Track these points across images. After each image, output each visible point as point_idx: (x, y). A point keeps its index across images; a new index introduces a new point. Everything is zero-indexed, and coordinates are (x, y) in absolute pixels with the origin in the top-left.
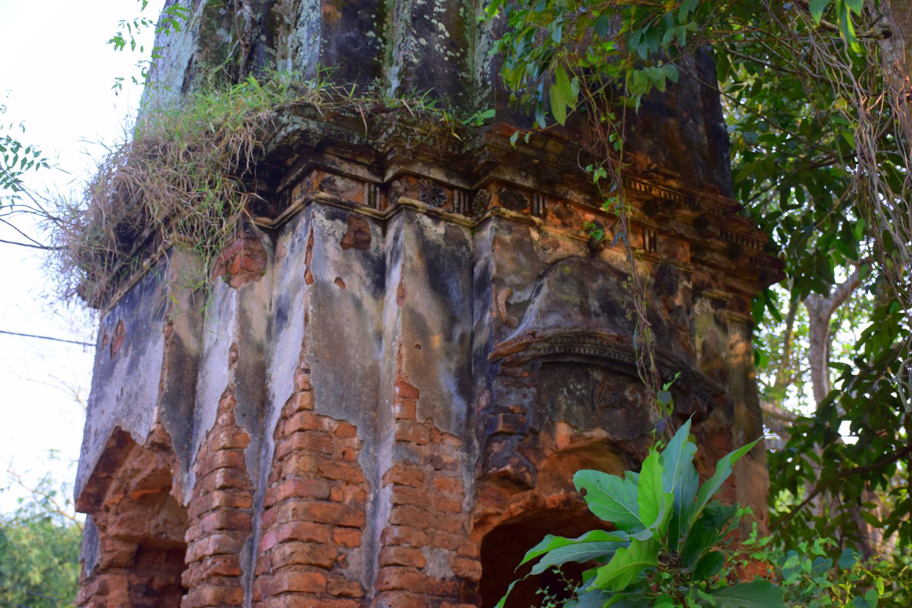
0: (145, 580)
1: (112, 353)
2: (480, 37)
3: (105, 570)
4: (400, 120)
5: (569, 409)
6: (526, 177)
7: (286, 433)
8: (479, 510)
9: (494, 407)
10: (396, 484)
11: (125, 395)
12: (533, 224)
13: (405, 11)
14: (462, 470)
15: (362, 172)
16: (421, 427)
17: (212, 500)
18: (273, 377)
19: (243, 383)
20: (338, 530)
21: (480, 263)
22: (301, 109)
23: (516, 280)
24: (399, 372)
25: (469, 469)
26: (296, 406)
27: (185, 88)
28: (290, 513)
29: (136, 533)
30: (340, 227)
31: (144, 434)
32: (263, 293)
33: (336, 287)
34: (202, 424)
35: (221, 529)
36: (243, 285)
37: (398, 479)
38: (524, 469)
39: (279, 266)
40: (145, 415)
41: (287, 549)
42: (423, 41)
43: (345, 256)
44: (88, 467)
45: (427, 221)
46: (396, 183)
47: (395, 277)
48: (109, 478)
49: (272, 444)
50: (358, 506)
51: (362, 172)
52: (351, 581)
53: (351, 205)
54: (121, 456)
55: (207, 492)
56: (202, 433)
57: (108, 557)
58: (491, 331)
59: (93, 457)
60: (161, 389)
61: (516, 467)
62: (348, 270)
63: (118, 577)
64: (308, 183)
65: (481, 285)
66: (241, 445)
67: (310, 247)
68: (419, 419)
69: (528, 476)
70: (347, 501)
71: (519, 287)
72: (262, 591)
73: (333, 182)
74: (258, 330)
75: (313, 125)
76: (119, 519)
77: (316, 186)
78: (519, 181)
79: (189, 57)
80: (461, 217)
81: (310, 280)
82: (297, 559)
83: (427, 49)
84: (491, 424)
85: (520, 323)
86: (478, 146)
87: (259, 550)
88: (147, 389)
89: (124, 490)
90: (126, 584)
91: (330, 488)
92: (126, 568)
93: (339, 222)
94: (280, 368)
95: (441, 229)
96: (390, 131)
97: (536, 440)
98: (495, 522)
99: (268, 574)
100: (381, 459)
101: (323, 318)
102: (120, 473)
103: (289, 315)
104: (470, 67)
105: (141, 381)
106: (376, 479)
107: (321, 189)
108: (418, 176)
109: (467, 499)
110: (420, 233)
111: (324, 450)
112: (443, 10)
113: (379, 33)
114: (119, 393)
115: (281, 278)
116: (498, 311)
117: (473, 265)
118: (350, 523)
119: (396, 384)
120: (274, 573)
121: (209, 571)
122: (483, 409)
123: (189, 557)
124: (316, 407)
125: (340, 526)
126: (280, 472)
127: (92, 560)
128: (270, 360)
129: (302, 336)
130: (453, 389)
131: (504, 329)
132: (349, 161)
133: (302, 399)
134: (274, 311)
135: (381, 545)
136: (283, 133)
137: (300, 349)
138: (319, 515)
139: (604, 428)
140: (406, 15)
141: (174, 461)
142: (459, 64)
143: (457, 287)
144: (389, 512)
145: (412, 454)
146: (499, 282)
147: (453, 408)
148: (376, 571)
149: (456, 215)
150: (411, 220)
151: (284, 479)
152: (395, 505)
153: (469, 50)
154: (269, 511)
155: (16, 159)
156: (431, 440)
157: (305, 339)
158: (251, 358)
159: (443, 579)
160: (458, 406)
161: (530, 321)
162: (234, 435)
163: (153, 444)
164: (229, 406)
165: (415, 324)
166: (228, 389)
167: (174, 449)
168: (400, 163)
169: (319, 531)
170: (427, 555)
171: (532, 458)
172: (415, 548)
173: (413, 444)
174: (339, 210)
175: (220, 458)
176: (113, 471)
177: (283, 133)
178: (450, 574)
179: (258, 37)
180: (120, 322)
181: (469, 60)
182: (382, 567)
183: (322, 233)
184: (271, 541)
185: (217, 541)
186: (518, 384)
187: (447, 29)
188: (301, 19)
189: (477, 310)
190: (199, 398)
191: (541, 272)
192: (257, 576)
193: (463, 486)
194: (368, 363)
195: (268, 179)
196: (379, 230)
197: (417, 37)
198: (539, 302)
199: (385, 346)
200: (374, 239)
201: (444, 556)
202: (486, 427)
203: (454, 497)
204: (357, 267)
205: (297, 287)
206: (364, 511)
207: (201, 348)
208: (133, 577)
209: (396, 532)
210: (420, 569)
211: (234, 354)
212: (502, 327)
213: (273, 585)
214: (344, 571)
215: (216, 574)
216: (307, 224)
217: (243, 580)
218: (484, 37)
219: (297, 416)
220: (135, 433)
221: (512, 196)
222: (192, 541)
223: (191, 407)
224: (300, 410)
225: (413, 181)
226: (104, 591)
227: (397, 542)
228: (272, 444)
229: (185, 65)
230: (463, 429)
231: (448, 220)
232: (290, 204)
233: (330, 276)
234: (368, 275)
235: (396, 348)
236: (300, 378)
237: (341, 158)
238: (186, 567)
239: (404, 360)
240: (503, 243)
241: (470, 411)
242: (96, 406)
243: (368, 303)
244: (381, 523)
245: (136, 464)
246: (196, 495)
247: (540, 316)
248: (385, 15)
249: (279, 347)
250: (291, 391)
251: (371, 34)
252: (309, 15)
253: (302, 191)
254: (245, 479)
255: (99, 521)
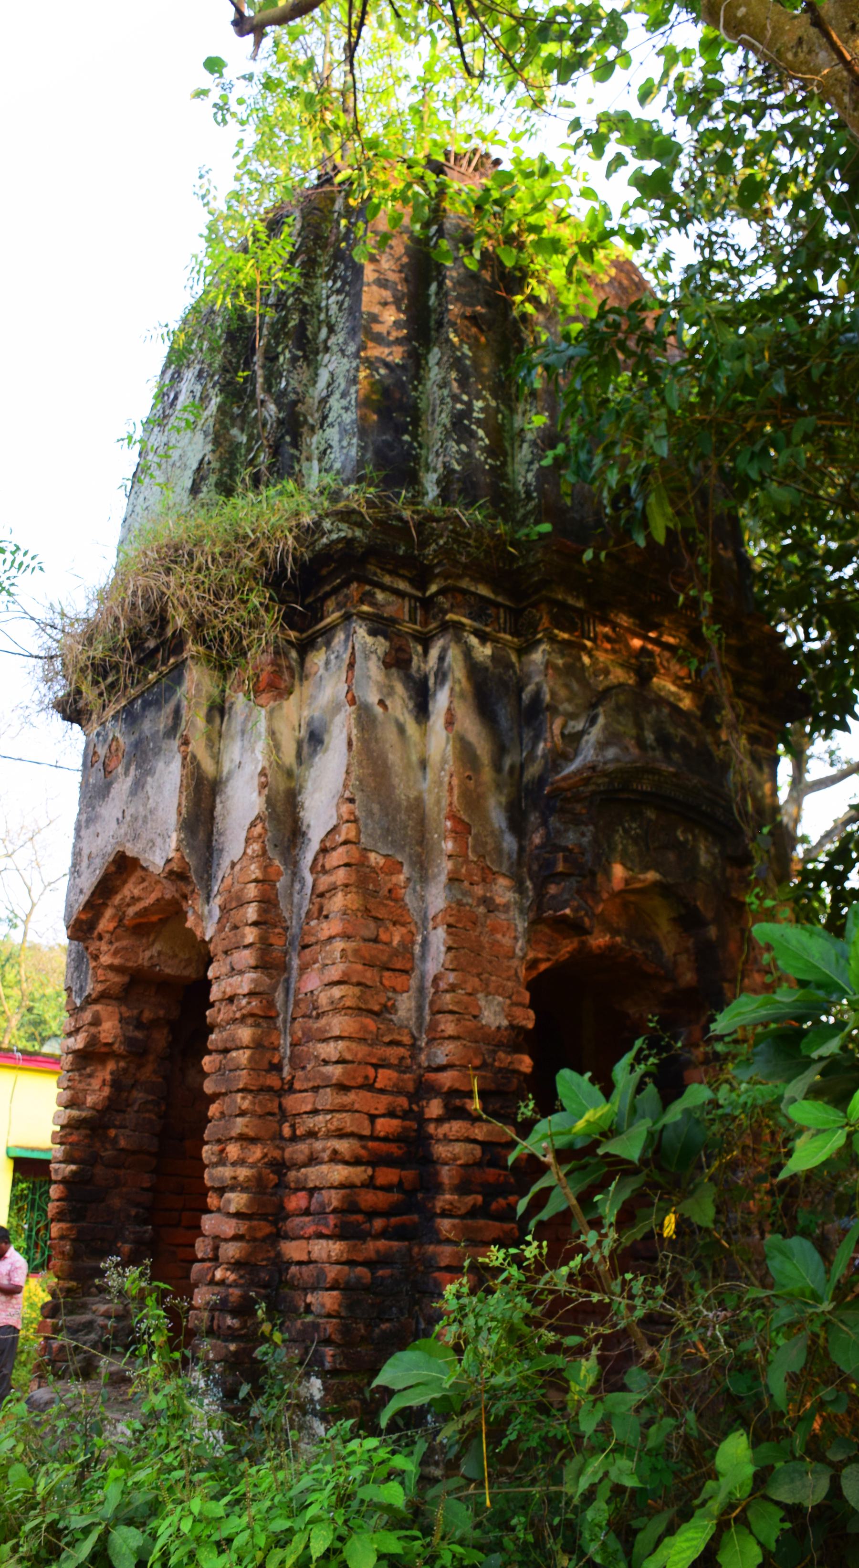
0: (135, 1012)
1: (107, 772)
2: (521, 447)
3: (96, 1001)
4: (453, 531)
5: (625, 850)
6: (577, 597)
7: (327, 867)
8: (531, 955)
9: (550, 845)
10: (449, 926)
11: (128, 818)
12: (584, 648)
13: (443, 415)
14: (514, 913)
15: (402, 585)
16: (473, 866)
17: (243, 936)
18: (306, 805)
19: (274, 810)
20: (387, 974)
21: (531, 688)
22: (347, 516)
23: (567, 707)
24: (451, 804)
25: (521, 911)
26: (341, 839)
27: (195, 490)
28: (337, 954)
29: (130, 964)
30: (381, 645)
31: (161, 863)
32: (294, 712)
33: (379, 710)
34: (225, 854)
35: (255, 968)
36: (272, 704)
37: (451, 920)
38: (582, 913)
39: (308, 687)
40: (159, 841)
41: (337, 992)
42: (464, 448)
43: (387, 676)
44: (81, 892)
45: (474, 641)
46: (441, 599)
47: (441, 701)
48: (105, 905)
49: (309, 879)
50: (406, 948)
51: (402, 585)
52: (401, 1027)
53: (393, 621)
54: (118, 883)
55: (235, 927)
56: (225, 863)
57: (100, 987)
58: (546, 763)
59: (89, 881)
60: (180, 814)
61: (575, 910)
62: (391, 692)
63: (110, 1008)
64: (346, 596)
65: (533, 714)
66: (273, 877)
67: (351, 665)
68: (472, 857)
69: (586, 920)
70: (395, 943)
71: (572, 716)
72: (304, 1034)
73: (373, 595)
74: (289, 756)
75: (358, 533)
76: (113, 948)
77: (356, 599)
78: (571, 601)
79: (200, 457)
80: (508, 637)
81: (353, 702)
82: (348, 1004)
83: (469, 455)
84: (549, 864)
85: (576, 755)
86: (532, 561)
87: (297, 991)
88: (160, 813)
89: (120, 920)
90: (117, 1016)
91: (378, 927)
92: (117, 999)
93: (381, 639)
94: (317, 796)
95: (488, 651)
96: (441, 542)
97: (594, 882)
98: (543, 967)
99: (310, 1017)
100: (430, 899)
101: (333, 744)
102: (117, 899)
103: (326, 738)
104: (511, 476)
105: (151, 804)
106: (425, 919)
107: (362, 602)
108: (464, 592)
109: (520, 943)
110: (468, 652)
111: (371, 886)
112: (482, 416)
113: (415, 437)
114: (120, 816)
115: (313, 697)
116: (553, 741)
117: (521, 690)
118: (398, 966)
119: (447, 818)
120: (318, 1016)
121: (244, 1011)
122: (537, 847)
123: (215, 993)
124: (363, 840)
125: (388, 969)
126: (321, 909)
127: (82, 989)
128: (301, 787)
129: (345, 762)
130: (504, 825)
131: (560, 761)
132: (391, 573)
133: (347, 831)
134: (304, 733)
135: (432, 990)
136: (324, 540)
137: (344, 776)
138: (367, 956)
139: (657, 870)
140: (445, 419)
141: (193, 891)
142: (499, 473)
143: (505, 714)
144: (442, 956)
145: (465, 894)
146: (553, 709)
147: (505, 845)
148: (428, 1018)
149: (502, 635)
150: (458, 639)
151: (326, 917)
152: (449, 949)
153: (509, 459)
154: (307, 951)
155: (13, 562)
156: (484, 880)
157: (349, 765)
158: (282, 785)
159: (499, 1028)
160: (509, 843)
161: (587, 753)
162: (266, 867)
163: (171, 872)
164: (260, 836)
165: (465, 752)
166: (258, 817)
167: (194, 878)
168: (446, 576)
169: (369, 974)
170: (482, 1003)
171: (590, 902)
172: (470, 994)
173: (466, 883)
174: (380, 626)
175: (252, 891)
176: (109, 898)
177: (324, 540)
178: (505, 1023)
179: (282, 437)
180: (115, 739)
181: (509, 470)
182: (434, 1013)
183: (364, 652)
184: (312, 982)
185: (253, 980)
186: (577, 821)
187: (487, 435)
188: (330, 420)
189: (526, 740)
190: (219, 825)
191: (594, 700)
192: (294, 1019)
193: (516, 930)
194: (413, 794)
195: (307, 589)
196: (420, 649)
197: (458, 443)
198: (595, 733)
199: (430, 775)
200: (415, 659)
201: (499, 1004)
202: (541, 867)
203: (507, 941)
204: (399, 688)
205: (337, 708)
206: (412, 954)
207: (219, 770)
208: (124, 1009)
209: (452, 977)
210: (475, 1017)
211: (263, 779)
212: (558, 758)
213: (318, 1029)
214: (393, 1017)
215: (252, 1015)
216: (347, 640)
217: (279, 1022)
218: (525, 446)
219: (341, 850)
220: (146, 860)
221: (565, 617)
222: (217, 978)
223: (211, 834)
224: (346, 842)
225: (460, 598)
226: (96, 1022)
227: (452, 988)
228: (309, 879)
229: (195, 466)
230: (515, 869)
231: (495, 640)
232: (322, 618)
233: (373, 698)
234: (410, 698)
235: (446, 779)
236: (345, 808)
237: (382, 569)
238: (212, 1005)
239: (456, 792)
240: (555, 667)
241: (521, 849)
242: (87, 827)
243: (412, 728)
244: (432, 967)
245: (136, 892)
246: (220, 930)
247: (595, 747)
248: (419, 419)
249: (313, 773)
250: (334, 822)
251: (406, 438)
252: (340, 416)
253: (338, 604)
254: (279, 915)
255: (91, 949)
